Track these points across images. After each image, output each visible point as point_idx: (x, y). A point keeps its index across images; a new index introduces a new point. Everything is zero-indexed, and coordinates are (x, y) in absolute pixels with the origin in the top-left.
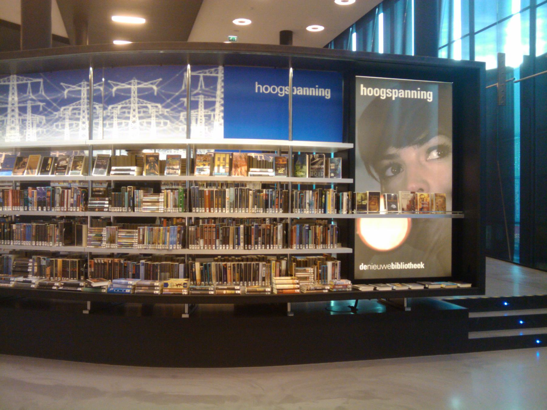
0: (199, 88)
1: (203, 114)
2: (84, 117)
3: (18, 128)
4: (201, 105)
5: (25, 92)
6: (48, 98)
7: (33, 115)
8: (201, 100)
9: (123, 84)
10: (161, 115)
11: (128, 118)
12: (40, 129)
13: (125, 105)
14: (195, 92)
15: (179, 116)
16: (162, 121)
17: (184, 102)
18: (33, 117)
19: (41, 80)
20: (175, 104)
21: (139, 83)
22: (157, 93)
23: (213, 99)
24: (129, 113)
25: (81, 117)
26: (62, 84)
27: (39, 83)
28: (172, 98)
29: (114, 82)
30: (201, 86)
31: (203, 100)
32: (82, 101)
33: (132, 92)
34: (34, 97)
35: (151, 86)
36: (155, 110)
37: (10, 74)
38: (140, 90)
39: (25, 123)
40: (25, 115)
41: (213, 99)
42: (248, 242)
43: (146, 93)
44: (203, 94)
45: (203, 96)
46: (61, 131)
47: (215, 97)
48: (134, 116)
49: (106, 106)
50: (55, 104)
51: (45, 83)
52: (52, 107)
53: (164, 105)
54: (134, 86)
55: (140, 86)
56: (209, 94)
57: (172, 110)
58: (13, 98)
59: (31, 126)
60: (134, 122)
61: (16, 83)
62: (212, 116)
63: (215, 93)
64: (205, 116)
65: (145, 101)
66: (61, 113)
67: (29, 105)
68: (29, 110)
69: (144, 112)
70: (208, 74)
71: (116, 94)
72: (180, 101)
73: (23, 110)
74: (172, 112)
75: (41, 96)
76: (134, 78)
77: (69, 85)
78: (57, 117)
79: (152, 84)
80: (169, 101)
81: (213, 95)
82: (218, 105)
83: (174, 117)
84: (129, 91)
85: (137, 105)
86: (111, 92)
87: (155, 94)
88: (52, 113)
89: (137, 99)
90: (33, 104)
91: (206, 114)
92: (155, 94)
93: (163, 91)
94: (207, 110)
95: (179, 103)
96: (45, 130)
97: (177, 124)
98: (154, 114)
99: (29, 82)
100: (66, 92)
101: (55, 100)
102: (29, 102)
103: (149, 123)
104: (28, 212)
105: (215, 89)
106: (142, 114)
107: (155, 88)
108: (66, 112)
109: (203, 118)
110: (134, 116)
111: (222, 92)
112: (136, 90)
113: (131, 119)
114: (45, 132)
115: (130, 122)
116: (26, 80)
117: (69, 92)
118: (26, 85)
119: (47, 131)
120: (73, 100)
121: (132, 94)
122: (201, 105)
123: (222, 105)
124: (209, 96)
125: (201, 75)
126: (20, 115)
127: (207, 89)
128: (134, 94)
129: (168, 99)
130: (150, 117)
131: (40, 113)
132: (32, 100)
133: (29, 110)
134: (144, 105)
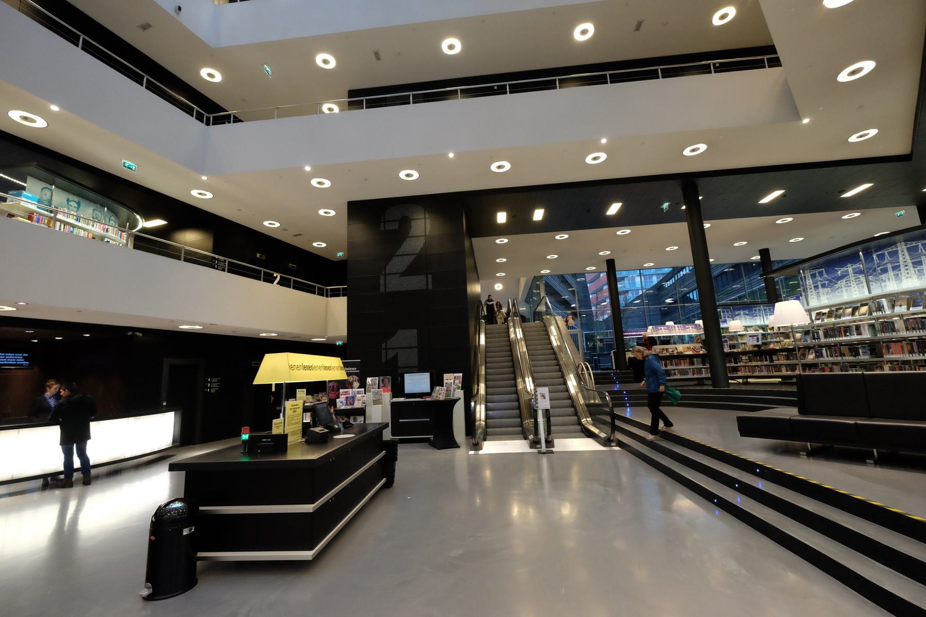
0: (886, 260)
3: (815, 297)
5: (823, 276)
6: (830, 278)
8: (889, 266)
12: (828, 296)
19: (823, 269)
21: (852, 266)
23: (898, 264)
24: (850, 283)
30: (887, 258)
35: (859, 266)
40: (921, 266)
41: (913, 261)
42: (693, 374)
47: (899, 262)
48: (853, 284)
55: (853, 267)
56: (893, 261)
57: (874, 276)
58: (809, 282)
60: (854, 287)
62: (899, 274)
67: (819, 284)
68: (820, 286)
69: (859, 281)
70: (890, 250)
73: (816, 287)
75: (825, 278)
78: (837, 287)
80: (871, 271)
83: (876, 280)
88: (833, 286)
89: (853, 275)
100: (839, 272)
101: (834, 278)
105: (898, 257)
106: (857, 282)
108: (842, 283)
109: (893, 277)
110: (853, 284)
115: (852, 288)
117: (841, 272)
119: (833, 296)
124: (894, 263)
126: (815, 290)
129: (870, 270)
130: (862, 283)
131: (827, 287)
132: (820, 281)
133: (820, 286)
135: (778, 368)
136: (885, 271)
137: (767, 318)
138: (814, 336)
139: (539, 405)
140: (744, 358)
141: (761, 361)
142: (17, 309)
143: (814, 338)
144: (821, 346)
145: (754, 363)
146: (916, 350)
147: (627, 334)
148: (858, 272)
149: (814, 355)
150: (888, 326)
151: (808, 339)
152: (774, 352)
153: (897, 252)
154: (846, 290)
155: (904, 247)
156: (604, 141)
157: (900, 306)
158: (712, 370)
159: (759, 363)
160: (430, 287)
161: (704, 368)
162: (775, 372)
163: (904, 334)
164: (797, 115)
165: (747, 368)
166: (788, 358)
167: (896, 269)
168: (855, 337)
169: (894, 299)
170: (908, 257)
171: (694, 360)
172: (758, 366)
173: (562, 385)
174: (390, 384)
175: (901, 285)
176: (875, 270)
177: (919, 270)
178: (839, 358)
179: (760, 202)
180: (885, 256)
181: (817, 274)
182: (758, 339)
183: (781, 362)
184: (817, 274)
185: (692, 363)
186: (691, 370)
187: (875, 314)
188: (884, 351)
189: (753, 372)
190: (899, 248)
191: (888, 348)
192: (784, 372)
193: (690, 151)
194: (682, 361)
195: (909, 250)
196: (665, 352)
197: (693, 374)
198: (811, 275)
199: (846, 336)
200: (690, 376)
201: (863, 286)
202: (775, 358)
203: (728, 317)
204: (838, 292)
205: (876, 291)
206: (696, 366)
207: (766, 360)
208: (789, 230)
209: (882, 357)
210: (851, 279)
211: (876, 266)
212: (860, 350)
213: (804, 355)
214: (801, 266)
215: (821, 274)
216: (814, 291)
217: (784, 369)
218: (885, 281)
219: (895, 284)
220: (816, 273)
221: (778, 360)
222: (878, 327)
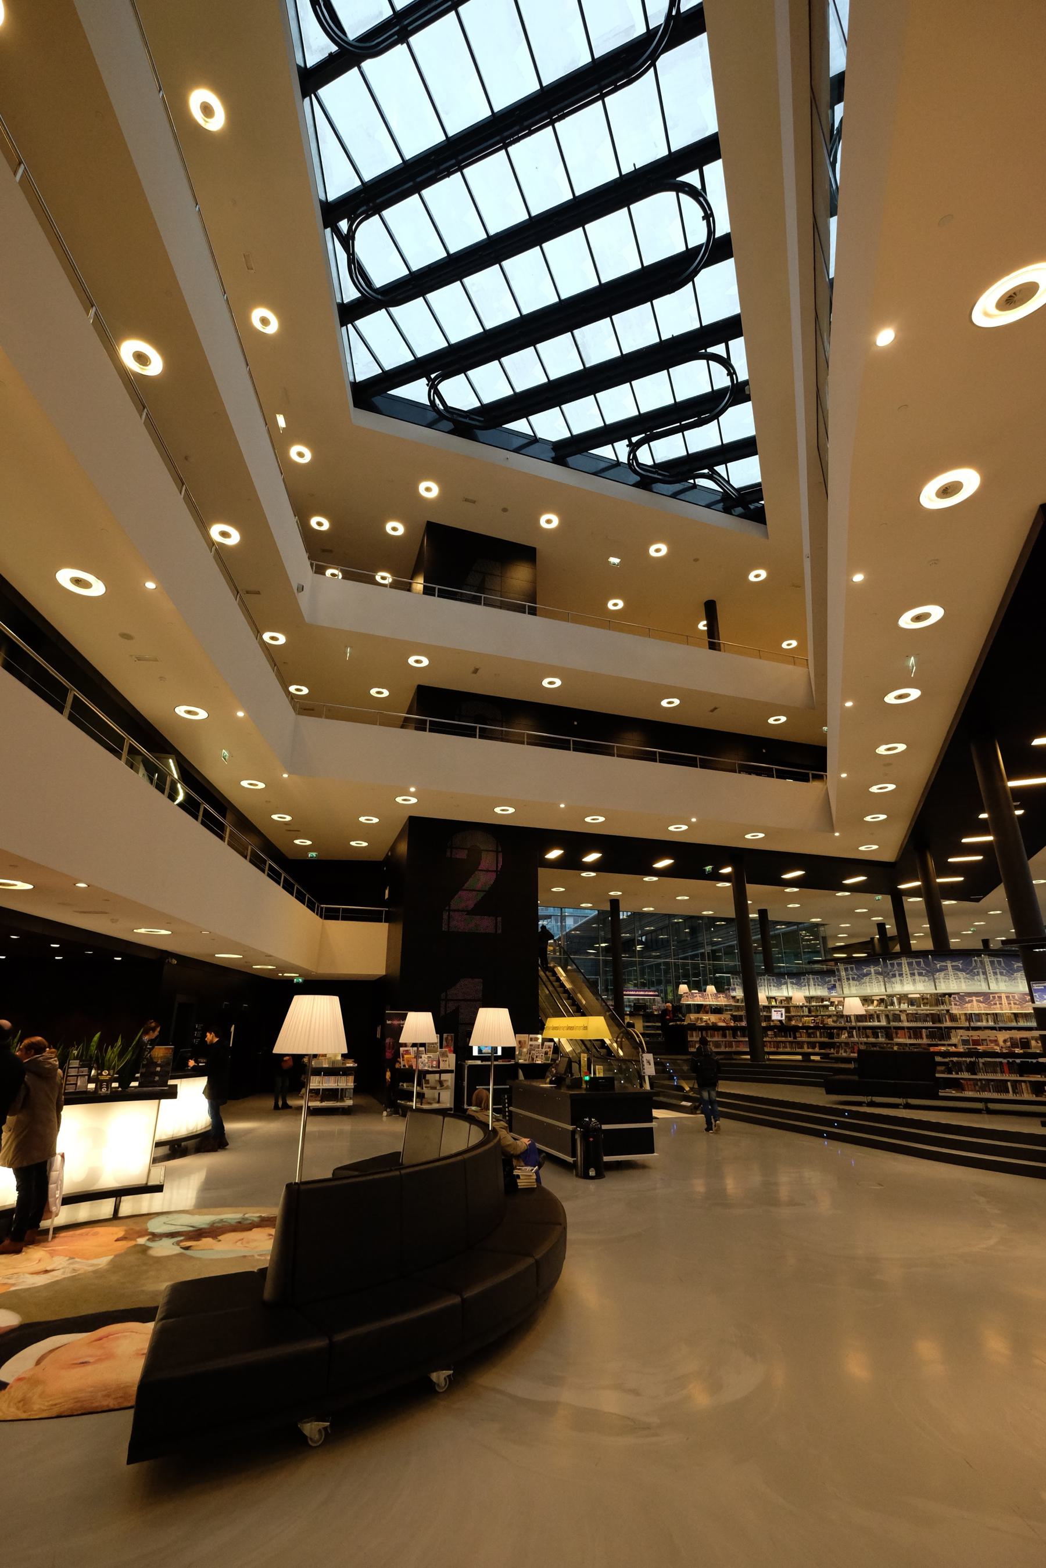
4: (897, 975)
16: (967, 980)
42: (726, 1047)
47: (902, 971)
48: (952, 978)
54: (949, 964)
73: (848, 979)
80: (968, 971)
100: (865, 971)
103: (961, 982)
107: (959, 965)
118: (847, 968)
120: (868, 974)
122: (897, 975)
125: (872, 970)
130: (960, 978)
131: (856, 980)
135: (800, 1045)
136: (894, 976)
137: (771, 989)
138: (847, 1019)
139: (645, 1071)
140: (769, 1033)
141: (786, 1037)
142: (172, 932)
143: (847, 1022)
144: (854, 1028)
145: (779, 1039)
146: (912, 1037)
147: (628, 993)
148: (877, 973)
149: (846, 1035)
150: (897, 1018)
151: (842, 1022)
152: (796, 1029)
153: (901, 963)
154: (870, 985)
155: (906, 961)
156: (694, 820)
157: (904, 1003)
158: (752, 1043)
159: (783, 1039)
160: (499, 931)
161: (734, 1041)
162: (798, 1048)
163: (906, 1024)
164: (833, 830)
165: (772, 1043)
166: (809, 1036)
168: (876, 1024)
169: (903, 998)
170: (907, 969)
171: (726, 1033)
172: (782, 1042)
174: (453, 1043)
176: (888, 974)
178: (865, 1039)
181: (849, 969)
182: (782, 1014)
183: (803, 1039)
184: (849, 969)
185: (724, 1036)
186: (724, 1042)
187: (889, 1007)
188: (894, 1035)
189: (778, 1047)
191: (897, 1034)
192: (806, 1050)
194: (716, 1033)
195: (908, 963)
196: (699, 1022)
197: (726, 1047)
199: (870, 1022)
200: (723, 1049)
202: (798, 1035)
203: (737, 985)
205: (890, 991)
206: (728, 1039)
207: (790, 1037)
208: (792, 898)
209: (893, 1040)
212: (879, 1034)
213: (839, 1036)
217: (805, 1046)
218: (894, 983)
221: (801, 1037)
222: (891, 1017)
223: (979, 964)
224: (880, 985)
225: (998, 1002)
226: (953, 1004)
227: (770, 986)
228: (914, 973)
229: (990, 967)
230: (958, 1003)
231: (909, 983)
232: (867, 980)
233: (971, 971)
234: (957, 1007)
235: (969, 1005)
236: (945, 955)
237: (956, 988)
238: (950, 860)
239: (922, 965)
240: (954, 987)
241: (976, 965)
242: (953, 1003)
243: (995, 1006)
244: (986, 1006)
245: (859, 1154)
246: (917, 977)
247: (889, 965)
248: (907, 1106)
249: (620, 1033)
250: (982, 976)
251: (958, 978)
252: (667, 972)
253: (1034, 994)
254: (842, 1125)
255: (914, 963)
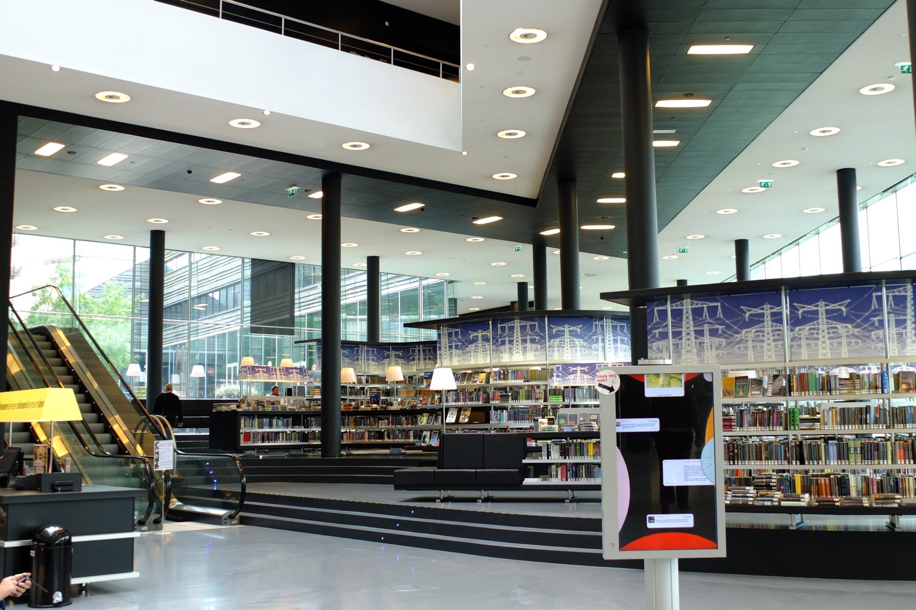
1: (895, 332)
2: (768, 339)
3: (521, 352)
6: (463, 340)
7: (712, 338)
9: (810, 307)
10: (852, 335)
11: (763, 341)
12: (459, 358)
13: (813, 327)
14: (504, 335)
15: (871, 335)
16: (583, 349)
17: (874, 322)
18: (711, 340)
20: (866, 323)
22: (846, 314)
23: (904, 318)
24: (818, 334)
25: (479, 350)
26: (469, 332)
27: (536, 324)
28: (862, 318)
29: (747, 308)
31: (893, 318)
32: (765, 323)
33: (820, 314)
34: (456, 340)
35: (576, 329)
36: (579, 343)
37: (514, 320)
38: (483, 336)
39: (703, 346)
40: (702, 338)
43: (835, 314)
44: (893, 313)
45: (893, 315)
46: (796, 351)
47: (906, 315)
48: (480, 350)
49: (793, 328)
50: (466, 344)
51: (722, 306)
52: (733, 330)
53: (853, 325)
54: (822, 307)
56: (899, 312)
57: (588, 343)
59: (710, 348)
61: (690, 307)
62: (904, 334)
63: (906, 311)
64: (897, 334)
65: (834, 322)
66: (796, 333)
68: (529, 341)
69: (834, 332)
70: (897, 294)
71: (802, 316)
72: (652, 333)
73: (524, 341)
74: (863, 331)
75: (459, 339)
76: (821, 300)
77: (751, 309)
78: (738, 339)
79: (840, 305)
81: (679, 325)
82: (909, 323)
83: (865, 336)
84: (477, 337)
85: (770, 329)
86: (745, 317)
87: (845, 314)
89: (825, 320)
90: (710, 328)
91: (898, 332)
92: (845, 314)
93: (852, 312)
94: (898, 329)
95: (870, 323)
96: (725, 352)
97: (869, 343)
98: (578, 345)
99: (705, 306)
101: (466, 341)
102: (454, 342)
104: (879, 465)
105: (905, 307)
110: (480, 350)
111: (912, 310)
112: (824, 311)
113: (820, 340)
114: (726, 355)
116: (702, 304)
117: (473, 336)
120: (475, 340)
121: (820, 316)
123: (913, 322)
124: (899, 315)
125: (480, 335)
126: (522, 344)
127: (897, 308)
128: (480, 338)
129: (859, 318)
132: (455, 341)
133: (529, 341)
134: (833, 326)
148: (835, 316)
154: (558, 350)
167: (901, 325)
170: (691, 322)
173: (53, 357)
175: (904, 351)
177: (524, 347)
179: (502, 218)
180: (703, 311)
190: (515, 325)
193: (536, 36)
198: (521, 326)
201: (577, 350)
204: (739, 348)
210: (766, 329)
211: (498, 337)
214: (442, 324)
215: (456, 333)
216: (520, 344)
219: (896, 347)
220: (527, 325)
223: (599, 328)
224: (487, 354)
225: (274, 373)
226: (555, 376)
227: (368, 360)
228: (703, 331)
229: (611, 334)
230: (285, 374)
231: (518, 352)
232: (473, 348)
233: (590, 337)
234: (559, 379)
235: (572, 377)
236: (563, 317)
237: (570, 358)
238: (600, 201)
239: (537, 329)
240: (568, 357)
241: (596, 329)
242: (555, 374)
243: (305, 377)
244: (590, 377)
245: (413, 557)
246: (529, 345)
247: (499, 329)
248: (487, 500)
249: (141, 423)
250: (600, 344)
251: (573, 346)
252: (202, 344)
253: (820, 356)
254: (405, 526)
255: (528, 327)
